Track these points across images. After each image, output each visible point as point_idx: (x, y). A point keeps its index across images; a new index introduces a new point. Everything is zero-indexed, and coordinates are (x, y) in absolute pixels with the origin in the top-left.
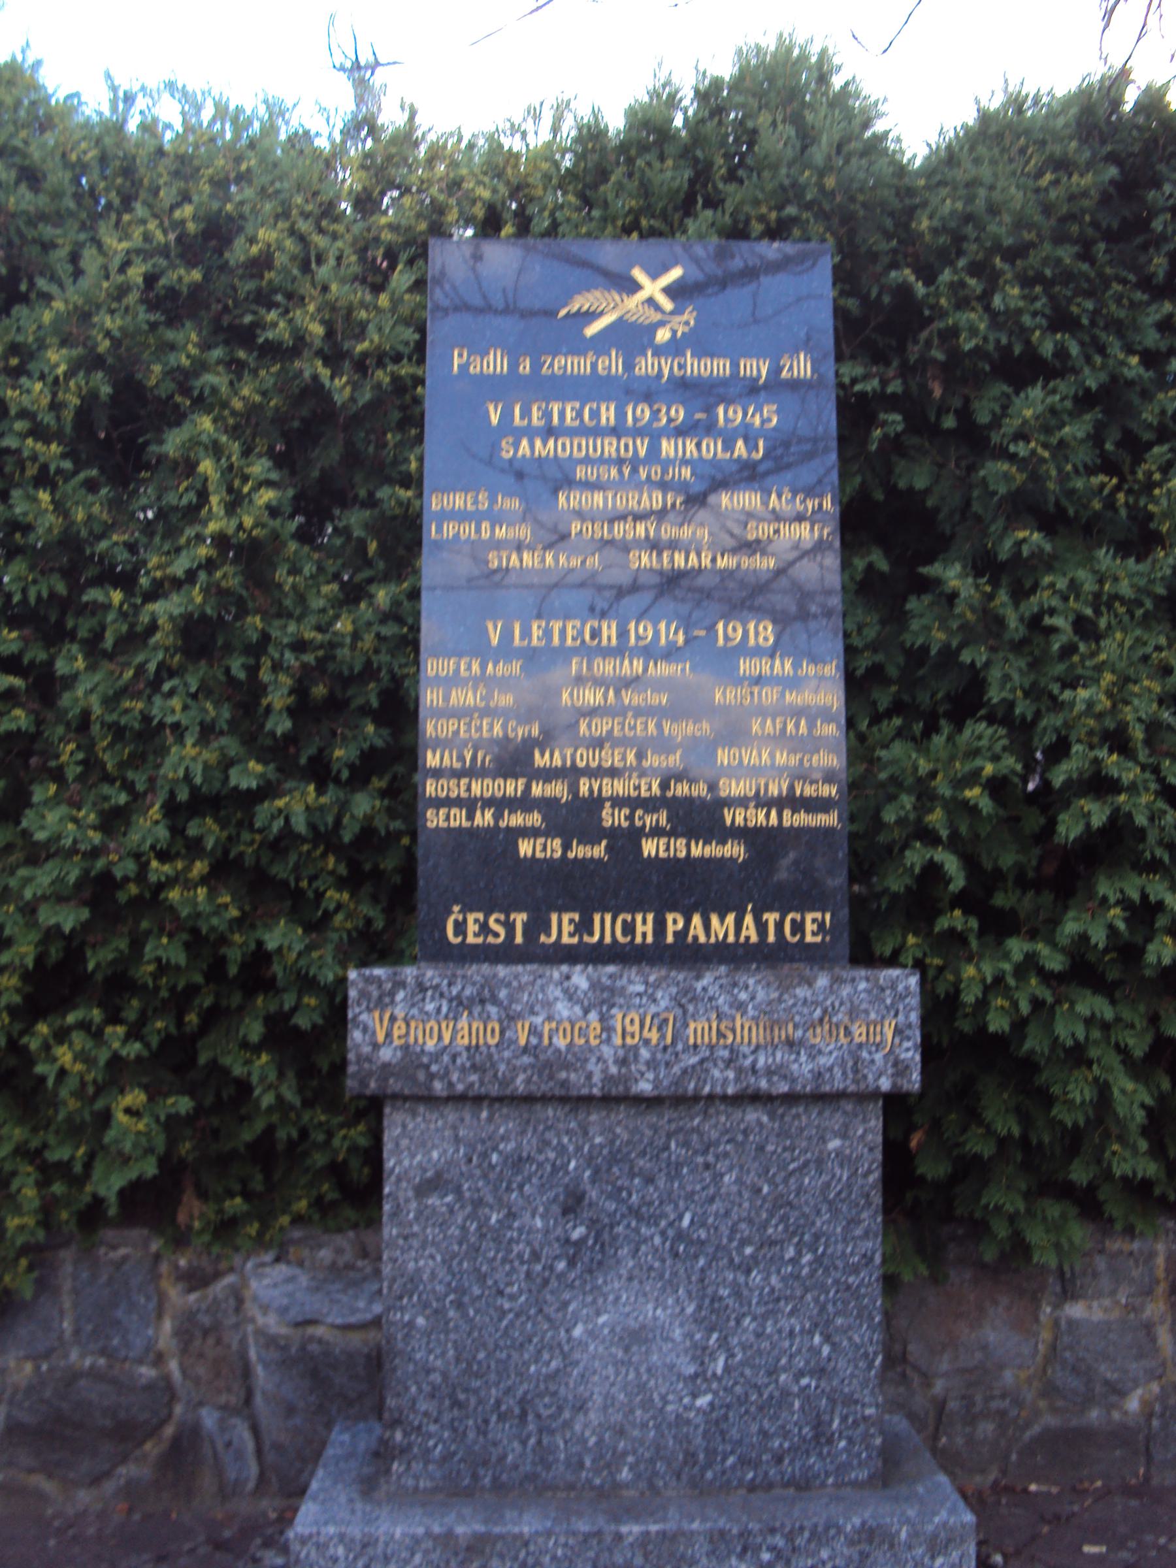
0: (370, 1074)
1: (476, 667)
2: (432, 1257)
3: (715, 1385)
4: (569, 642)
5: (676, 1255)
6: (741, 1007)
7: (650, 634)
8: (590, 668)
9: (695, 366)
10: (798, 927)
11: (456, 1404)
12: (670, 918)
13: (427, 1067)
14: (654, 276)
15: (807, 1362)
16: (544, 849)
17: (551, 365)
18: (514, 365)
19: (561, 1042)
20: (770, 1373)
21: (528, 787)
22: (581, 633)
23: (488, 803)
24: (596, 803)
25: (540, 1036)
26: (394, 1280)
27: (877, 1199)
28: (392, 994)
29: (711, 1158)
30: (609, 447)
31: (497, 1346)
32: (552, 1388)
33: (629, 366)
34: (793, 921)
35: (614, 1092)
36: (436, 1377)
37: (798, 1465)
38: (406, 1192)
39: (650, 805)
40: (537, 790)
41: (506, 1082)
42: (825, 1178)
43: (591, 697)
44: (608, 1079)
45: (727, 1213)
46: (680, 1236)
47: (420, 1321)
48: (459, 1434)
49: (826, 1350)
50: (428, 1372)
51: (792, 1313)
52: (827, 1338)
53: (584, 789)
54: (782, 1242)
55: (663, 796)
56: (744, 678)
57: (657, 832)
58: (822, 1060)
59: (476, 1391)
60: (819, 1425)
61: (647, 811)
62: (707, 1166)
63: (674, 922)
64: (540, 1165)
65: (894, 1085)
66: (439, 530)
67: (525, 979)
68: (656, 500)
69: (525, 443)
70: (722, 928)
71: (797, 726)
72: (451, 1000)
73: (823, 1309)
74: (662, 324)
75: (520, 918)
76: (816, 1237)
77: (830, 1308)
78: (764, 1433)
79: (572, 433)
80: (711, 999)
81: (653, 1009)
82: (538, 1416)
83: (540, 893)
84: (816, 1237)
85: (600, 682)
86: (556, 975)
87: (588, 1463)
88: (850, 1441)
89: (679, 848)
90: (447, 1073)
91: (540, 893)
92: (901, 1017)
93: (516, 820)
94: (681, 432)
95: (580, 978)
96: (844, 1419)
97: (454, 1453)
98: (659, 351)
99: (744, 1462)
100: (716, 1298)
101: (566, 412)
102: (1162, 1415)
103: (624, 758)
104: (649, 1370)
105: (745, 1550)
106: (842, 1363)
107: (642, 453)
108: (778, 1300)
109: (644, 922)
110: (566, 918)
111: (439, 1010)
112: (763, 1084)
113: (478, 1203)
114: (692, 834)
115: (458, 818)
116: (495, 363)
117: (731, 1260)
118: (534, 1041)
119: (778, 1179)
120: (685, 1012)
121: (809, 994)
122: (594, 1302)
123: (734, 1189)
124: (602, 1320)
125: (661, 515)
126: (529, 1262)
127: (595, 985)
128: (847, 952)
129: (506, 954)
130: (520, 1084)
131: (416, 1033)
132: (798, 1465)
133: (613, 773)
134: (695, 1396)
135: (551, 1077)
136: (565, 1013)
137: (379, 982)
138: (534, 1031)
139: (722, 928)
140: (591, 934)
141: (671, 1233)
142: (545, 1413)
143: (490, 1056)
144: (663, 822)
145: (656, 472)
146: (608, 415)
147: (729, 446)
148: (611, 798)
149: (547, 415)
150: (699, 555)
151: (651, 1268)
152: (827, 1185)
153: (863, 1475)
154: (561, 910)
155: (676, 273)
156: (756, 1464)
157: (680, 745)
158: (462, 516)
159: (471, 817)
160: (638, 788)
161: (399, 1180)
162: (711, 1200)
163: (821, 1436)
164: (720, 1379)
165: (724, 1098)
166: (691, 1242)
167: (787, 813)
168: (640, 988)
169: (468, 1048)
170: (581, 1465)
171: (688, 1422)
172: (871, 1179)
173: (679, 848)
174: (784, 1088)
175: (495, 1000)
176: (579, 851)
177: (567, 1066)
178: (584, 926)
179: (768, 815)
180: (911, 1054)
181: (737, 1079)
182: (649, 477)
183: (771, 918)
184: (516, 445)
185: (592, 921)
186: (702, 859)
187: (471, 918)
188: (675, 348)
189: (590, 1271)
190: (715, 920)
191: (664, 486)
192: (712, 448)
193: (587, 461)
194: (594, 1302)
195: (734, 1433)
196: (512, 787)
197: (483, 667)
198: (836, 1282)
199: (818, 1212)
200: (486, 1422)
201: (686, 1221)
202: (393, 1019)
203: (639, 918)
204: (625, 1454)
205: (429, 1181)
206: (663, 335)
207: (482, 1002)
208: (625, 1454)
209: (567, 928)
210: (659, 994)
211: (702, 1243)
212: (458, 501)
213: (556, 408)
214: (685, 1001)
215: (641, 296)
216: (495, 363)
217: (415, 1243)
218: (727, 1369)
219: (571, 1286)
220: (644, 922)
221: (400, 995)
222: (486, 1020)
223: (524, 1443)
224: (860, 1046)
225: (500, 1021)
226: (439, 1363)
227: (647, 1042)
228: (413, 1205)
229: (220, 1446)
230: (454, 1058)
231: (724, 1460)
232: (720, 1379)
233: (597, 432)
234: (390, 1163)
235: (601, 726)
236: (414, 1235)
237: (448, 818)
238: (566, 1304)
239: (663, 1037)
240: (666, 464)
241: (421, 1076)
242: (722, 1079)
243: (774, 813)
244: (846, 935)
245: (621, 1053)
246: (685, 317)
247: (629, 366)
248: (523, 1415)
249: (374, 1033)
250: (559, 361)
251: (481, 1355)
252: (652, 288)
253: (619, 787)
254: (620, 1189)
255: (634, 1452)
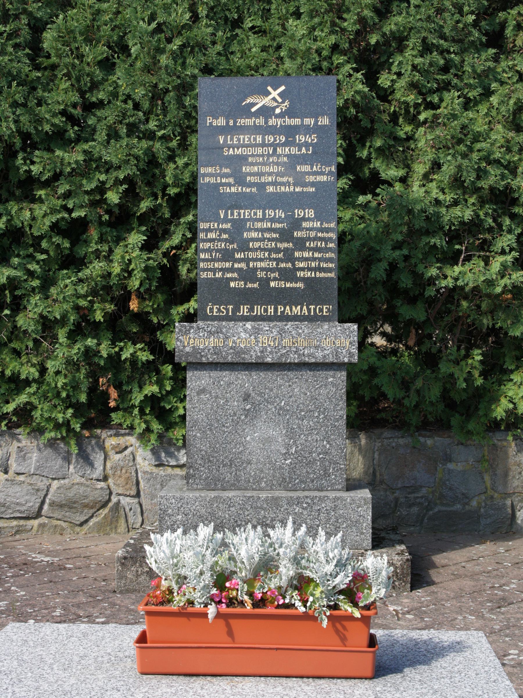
0: (183, 355)
1: (216, 225)
2: (202, 414)
3: (292, 457)
4: (246, 217)
5: (280, 414)
6: (299, 335)
7: (273, 214)
8: (253, 225)
9: (289, 121)
10: (321, 310)
11: (210, 461)
12: (279, 307)
13: (200, 353)
14: (275, 90)
15: (322, 450)
16: (238, 285)
17: (240, 123)
18: (227, 123)
19: (242, 346)
20: (310, 453)
21: (233, 265)
22: (250, 214)
23: (221, 270)
24: (256, 269)
25: (236, 344)
26: (190, 422)
27: (345, 398)
28: (189, 330)
29: (290, 383)
30: (260, 151)
31: (223, 443)
32: (240, 456)
33: (266, 122)
34: (319, 308)
35: (259, 361)
36: (203, 453)
37: (319, 482)
38: (194, 394)
39: (272, 270)
40: (236, 266)
41: (225, 358)
42: (327, 390)
43: (254, 235)
44: (257, 357)
45: (296, 401)
46: (281, 408)
47: (198, 435)
48: (211, 471)
49: (328, 446)
50: (201, 451)
51: (317, 434)
52: (328, 442)
53: (251, 265)
54: (314, 411)
55: (277, 268)
56: (304, 228)
57: (275, 279)
58: (326, 352)
59: (216, 457)
60: (325, 470)
61: (272, 273)
62: (290, 386)
63: (280, 309)
64: (236, 385)
65: (349, 360)
66: (203, 180)
67: (231, 326)
68: (275, 169)
69: (231, 149)
70: (296, 310)
71: (321, 244)
72: (208, 332)
73: (327, 433)
74: (277, 107)
75: (231, 307)
76: (325, 409)
77: (329, 433)
78: (307, 472)
79: (247, 146)
80: (290, 332)
81: (272, 335)
82: (236, 465)
83: (237, 299)
84: (325, 409)
85: (257, 230)
86: (241, 324)
87: (251, 481)
88: (336, 476)
89: (282, 284)
90: (207, 355)
91: (237, 299)
92: (351, 339)
93: (229, 275)
94: (285, 145)
95: (249, 325)
96: (334, 469)
97: (209, 477)
98: (277, 116)
99: (301, 482)
100: (293, 429)
101: (245, 139)
102: (485, 507)
103: (264, 256)
104: (271, 451)
105: (298, 503)
106: (333, 451)
107: (271, 153)
108: (312, 429)
109: (271, 308)
110: (245, 307)
111: (204, 335)
112: (307, 359)
113: (217, 397)
114: (287, 280)
115: (210, 275)
116: (221, 122)
117: (297, 416)
118: (234, 345)
119: (312, 391)
120: (282, 336)
121: (321, 331)
122: (253, 429)
123: (298, 393)
124: (255, 435)
125: (278, 174)
126: (233, 416)
127: (253, 327)
128: (337, 318)
129: (227, 318)
130: (229, 359)
131: (197, 342)
132: (319, 482)
133: (261, 260)
134: (285, 460)
135: (239, 357)
136: (244, 336)
137: (185, 327)
138: (234, 342)
139: (296, 310)
140: (253, 312)
141: (278, 407)
142: (238, 464)
143: (220, 349)
144: (277, 276)
145: (275, 159)
146: (259, 139)
147: (299, 150)
148: (260, 268)
149: (239, 140)
150: (289, 188)
151: (272, 418)
152: (329, 393)
153: (340, 487)
154: (244, 305)
155: (283, 88)
156: (305, 482)
157: (282, 251)
158: (210, 175)
159: (214, 275)
160: (269, 265)
161: (192, 390)
162: (291, 397)
163: (326, 474)
164: (293, 455)
165: (295, 364)
166: (284, 410)
167: (318, 273)
168: (268, 328)
169: (213, 347)
170: (249, 481)
171: (283, 468)
172: (343, 391)
173: (282, 284)
174: (313, 360)
175: (222, 332)
176: (249, 285)
177: (244, 353)
178: (251, 310)
179: (311, 274)
180: (355, 350)
181: (298, 358)
182: (273, 161)
183: (312, 307)
184: (228, 151)
185: (254, 308)
186: (289, 288)
187: (215, 307)
188: (281, 115)
189: (252, 419)
190: (294, 308)
191: (277, 164)
192: (294, 151)
193: (253, 155)
194: (253, 429)
195: (298, 472)
196: (228, 265)
197: (218, 225)
198: (331, 424)
199: (325, 402)
200: (219, 467)
201: (283, 404)
202: (190, 338)
203: (269, 307)
204: (263, 478)
205: (201, 390)
206: (278, 111)
207: (218, 333)
208: (263, 478)
209: (246, 310)
210: (274, 330)
211: (288, 411)
212: (210, 170)
213: (242, 137)
214: (282, 332)
215: (271, 97)
216: (221, 122)
217: (197, 410)
218: (296, 452)
219: (246, 424)
220: (271, 308)
221: (192, 331)
222: (219, 338)
223: (231, 474)
224: (338, 347)
225: (223, 339)
226: (204, 448)
227: (269, 345)
228: (196, 398)
229: (127, 509)
230: (209, 350)
231: (295, 480)
232: (293, 455)
233: (257, 145)
234: (188, 384)
235: (257, 245)
236: (196, 407)
237: (207, 275)
238: (244, 429)
239: (275, 344)
240: (279, 156)
241: (199, 356)
242: (294, 358)
243: (313, 273)
244: (337, 313)
245: (261, 349)
246: (286, 104)
247: (266, 122)
248: (231, 464)
249: (184, 342)
250: (243, 121)
251: (217, 446)
252: (274, 94)
253: (263, 265)
254: (262, 393)
255: (266, 477)
